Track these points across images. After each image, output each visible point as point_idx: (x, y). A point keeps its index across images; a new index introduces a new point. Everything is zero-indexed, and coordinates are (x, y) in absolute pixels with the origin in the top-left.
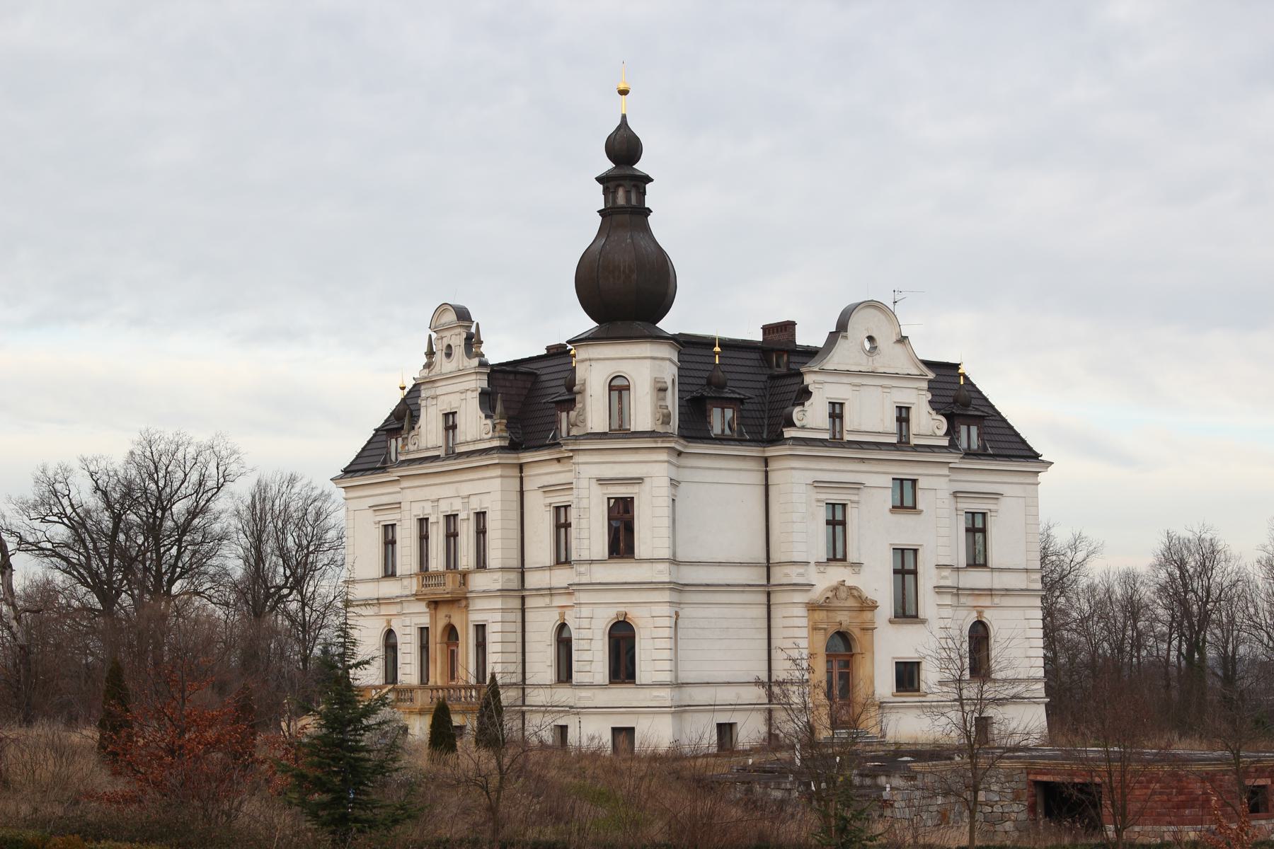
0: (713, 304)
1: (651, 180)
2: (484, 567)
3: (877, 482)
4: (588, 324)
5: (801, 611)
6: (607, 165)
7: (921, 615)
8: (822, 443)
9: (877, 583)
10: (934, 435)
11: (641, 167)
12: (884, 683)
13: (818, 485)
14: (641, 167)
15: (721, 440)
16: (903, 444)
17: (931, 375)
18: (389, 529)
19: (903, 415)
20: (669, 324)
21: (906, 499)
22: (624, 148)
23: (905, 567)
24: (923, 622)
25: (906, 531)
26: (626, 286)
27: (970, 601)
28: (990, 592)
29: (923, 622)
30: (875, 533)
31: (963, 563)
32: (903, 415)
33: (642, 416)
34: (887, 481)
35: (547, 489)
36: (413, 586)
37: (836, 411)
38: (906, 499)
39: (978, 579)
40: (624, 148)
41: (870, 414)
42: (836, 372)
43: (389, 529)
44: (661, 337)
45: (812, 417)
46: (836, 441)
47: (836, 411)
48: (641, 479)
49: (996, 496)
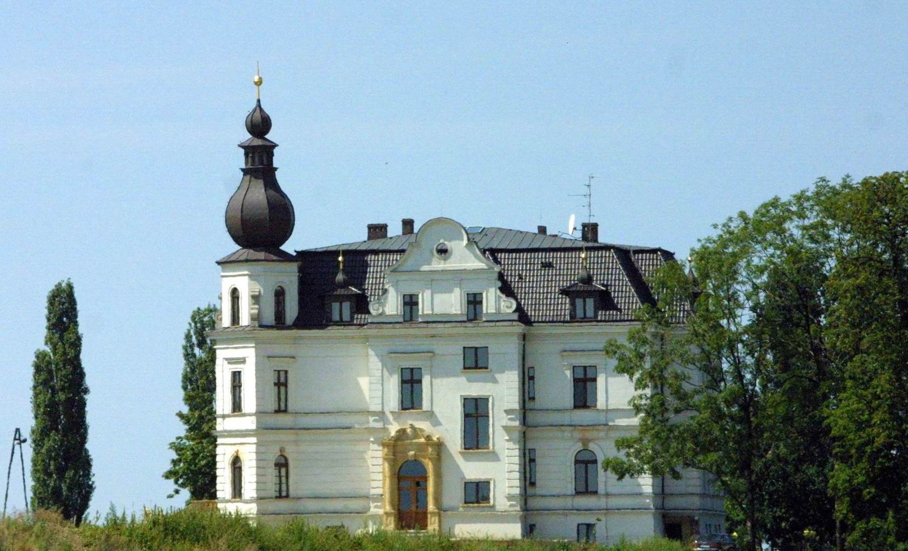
2: (240, 409)
6: (246, 137)
9: (451, 430)
10: (456, 315)
12: (454, 495)
19: (474, 301)
20: (290, 247)
22: (259, 125)
23: (475, 413)
26: (261, 227)
27: (577, 435)
32: (474, 301)
33: (245, 320)
35: (231, 361)
36: (250, 423)
37: (410, 302)
44: (286, 257)
47: (410, 302)
48: (244, 358)
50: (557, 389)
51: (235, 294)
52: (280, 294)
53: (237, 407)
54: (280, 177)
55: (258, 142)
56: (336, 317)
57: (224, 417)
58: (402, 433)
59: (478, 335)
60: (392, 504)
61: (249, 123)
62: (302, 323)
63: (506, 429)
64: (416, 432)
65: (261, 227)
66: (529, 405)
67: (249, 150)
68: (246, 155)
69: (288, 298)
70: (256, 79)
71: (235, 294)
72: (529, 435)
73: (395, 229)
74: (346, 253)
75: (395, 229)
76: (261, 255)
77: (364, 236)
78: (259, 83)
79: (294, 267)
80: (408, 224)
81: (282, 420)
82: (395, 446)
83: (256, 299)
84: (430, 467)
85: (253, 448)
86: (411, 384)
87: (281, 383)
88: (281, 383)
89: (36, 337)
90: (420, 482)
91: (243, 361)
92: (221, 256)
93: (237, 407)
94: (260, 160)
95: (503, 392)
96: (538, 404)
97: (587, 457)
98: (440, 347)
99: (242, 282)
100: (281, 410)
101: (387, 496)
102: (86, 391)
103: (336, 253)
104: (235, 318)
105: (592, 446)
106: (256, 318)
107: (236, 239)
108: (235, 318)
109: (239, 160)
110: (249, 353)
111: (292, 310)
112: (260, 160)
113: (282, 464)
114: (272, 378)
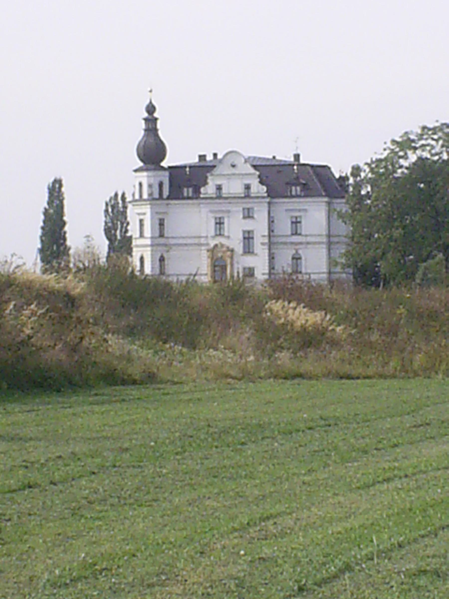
0: (177, 155)
1: (151, 102)
3: (237, 210)
4: (141, 164)
5: (205, 252)
6: (146, 115)
7: (256, 252)
8: (211, 198)
10: (240, 194)
11: (156, 115)
13: (211, 212)
14: (156, 115)
15: (189, 198)
16: (247, 196)
17: (258, 173)
18: (141, 221)
19: (248, 187)
20: (164, 164)
21: (248, 215)
22: (151, 109)
23: (248, 237)
24: (256, 255)
25: (249, 225)
26: (152, 152)
27: (294, 246)
28: (301, 243)
29: (256, 255)
30: (235, 227)
31: (289, 233)
32: (248, 187)
33: (145, 196)
34: (241, 209)
36: (149, 242)
37: (219, 188)
38: (248, 215)
39: (295, 239)
40: (151, 109)
41: (234, 187)
42: (218, 175)
43: (141, 221)
44: (163, 168)
45: (209, 189)
46: (219, 197)
47: (219, 188)
49: (305, 210)
50: (284, 227)
51: (141, 184)
52: (161, 185)
53: (142, 235)
54: (160, 133)
55: (150, 117)
56: (185, 194)
57: (136, 239)
58: (216, 246)
59: (249, 203)
60: (212, 277)
61: (141, 152)
62: (169, 198)
63: (263, 244)
64: (222, 246)
65: (152, 152)
66: (272, 234)
67: (146, 120)
68: (146, 123)
69: (164, 186)
70: (149, 89)
71: (141, 184)
72: (272, 246)
73: (210, 158)
74: (190, 167)
75: (210, 158)
76: (153, 167)
77: (197, 160)
78: (151, 91)
79: (167, 173)
80: (215, 155)
81: (162, 241)
82: (213, 251)
83: (150, 186)
84: (229, 261)
85: (149, 253)
86: (219, 223)
87: (161, 224)
88: (161, 224)
89: (42, 200)
90: (224, 268)
91: (144, 214)
92: (135, 168)
93: (142, 235)
94: (151, 122)
95: (260, 226)
96: (276, 233)
97: (297, 256)
98: (233, 208)
99: (144, 177)
100: (161, 235)
101: (209, 273)
102: (43, 228)
103: (185, 167)
104: (141, 196)
105: (300, 252)
106: (150, 195)
107: (142, 160)
108: (141, 196)
109: (143, 125)
110: (147, 209)
111: (166, 193)
112: (151, 122)
113: (162, 259)
114: (157, 222)
